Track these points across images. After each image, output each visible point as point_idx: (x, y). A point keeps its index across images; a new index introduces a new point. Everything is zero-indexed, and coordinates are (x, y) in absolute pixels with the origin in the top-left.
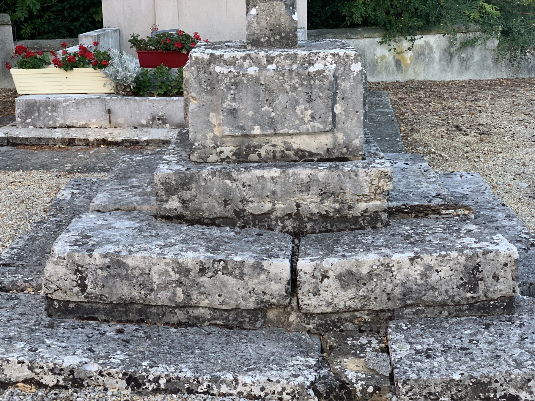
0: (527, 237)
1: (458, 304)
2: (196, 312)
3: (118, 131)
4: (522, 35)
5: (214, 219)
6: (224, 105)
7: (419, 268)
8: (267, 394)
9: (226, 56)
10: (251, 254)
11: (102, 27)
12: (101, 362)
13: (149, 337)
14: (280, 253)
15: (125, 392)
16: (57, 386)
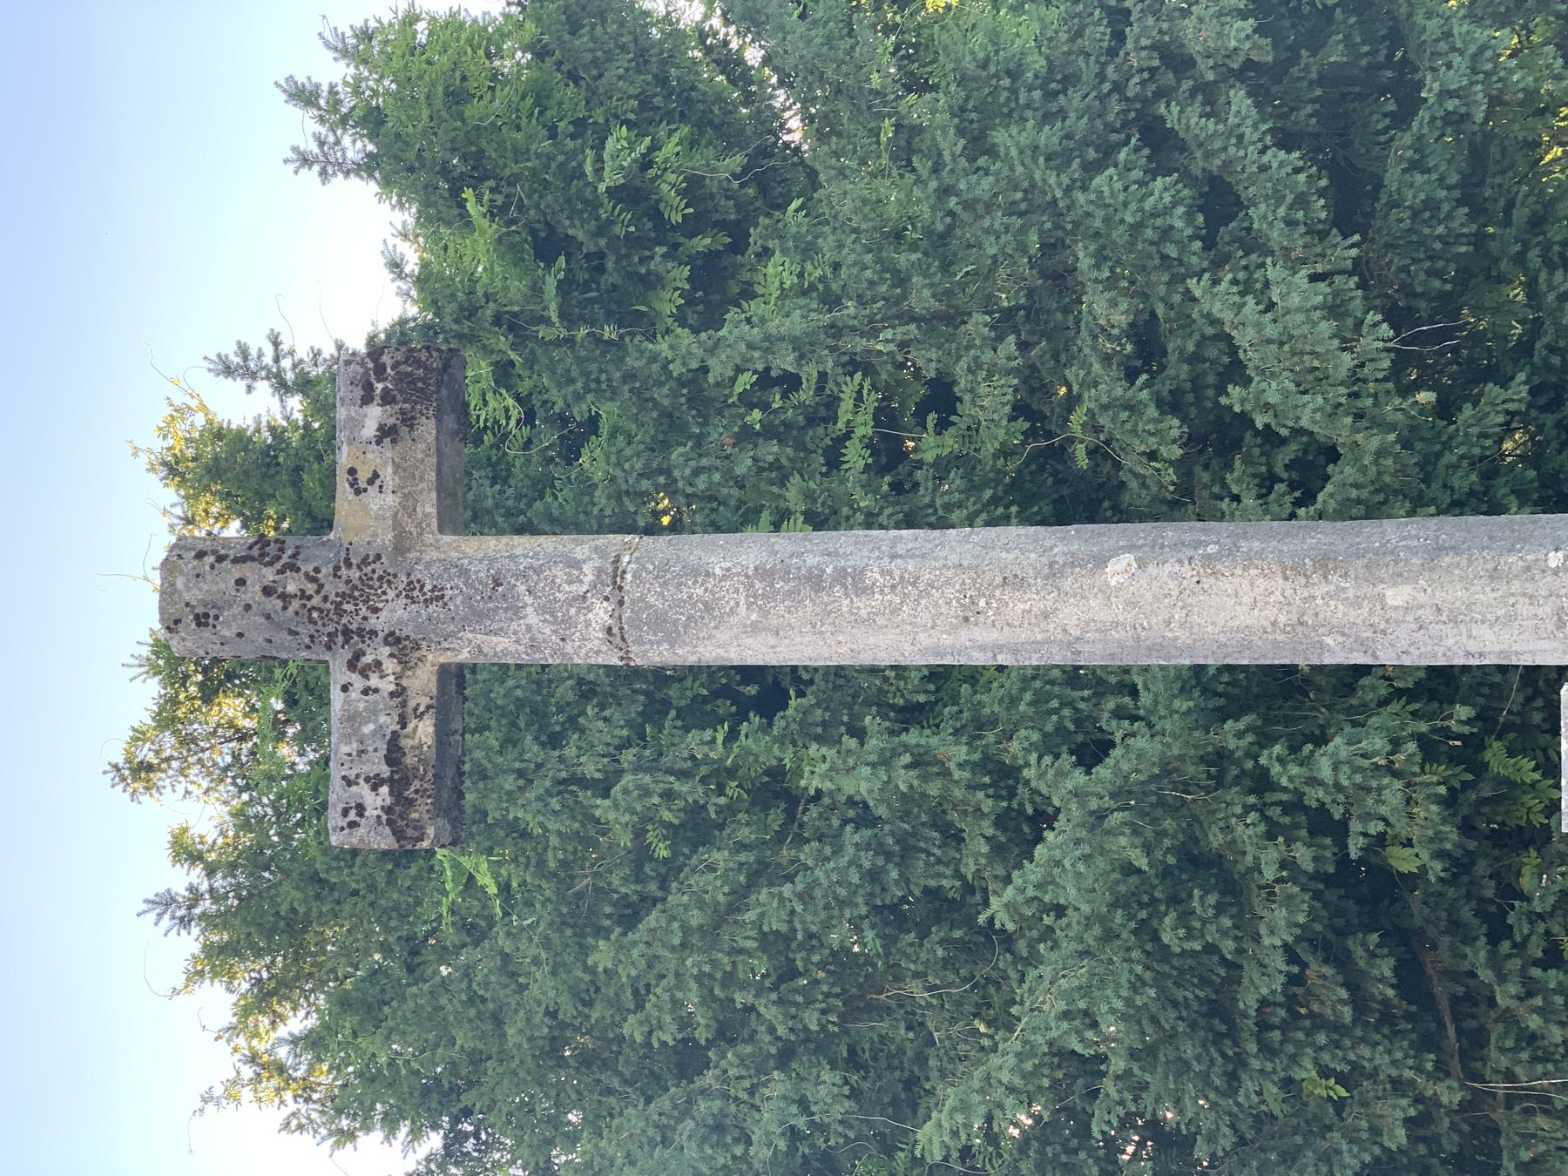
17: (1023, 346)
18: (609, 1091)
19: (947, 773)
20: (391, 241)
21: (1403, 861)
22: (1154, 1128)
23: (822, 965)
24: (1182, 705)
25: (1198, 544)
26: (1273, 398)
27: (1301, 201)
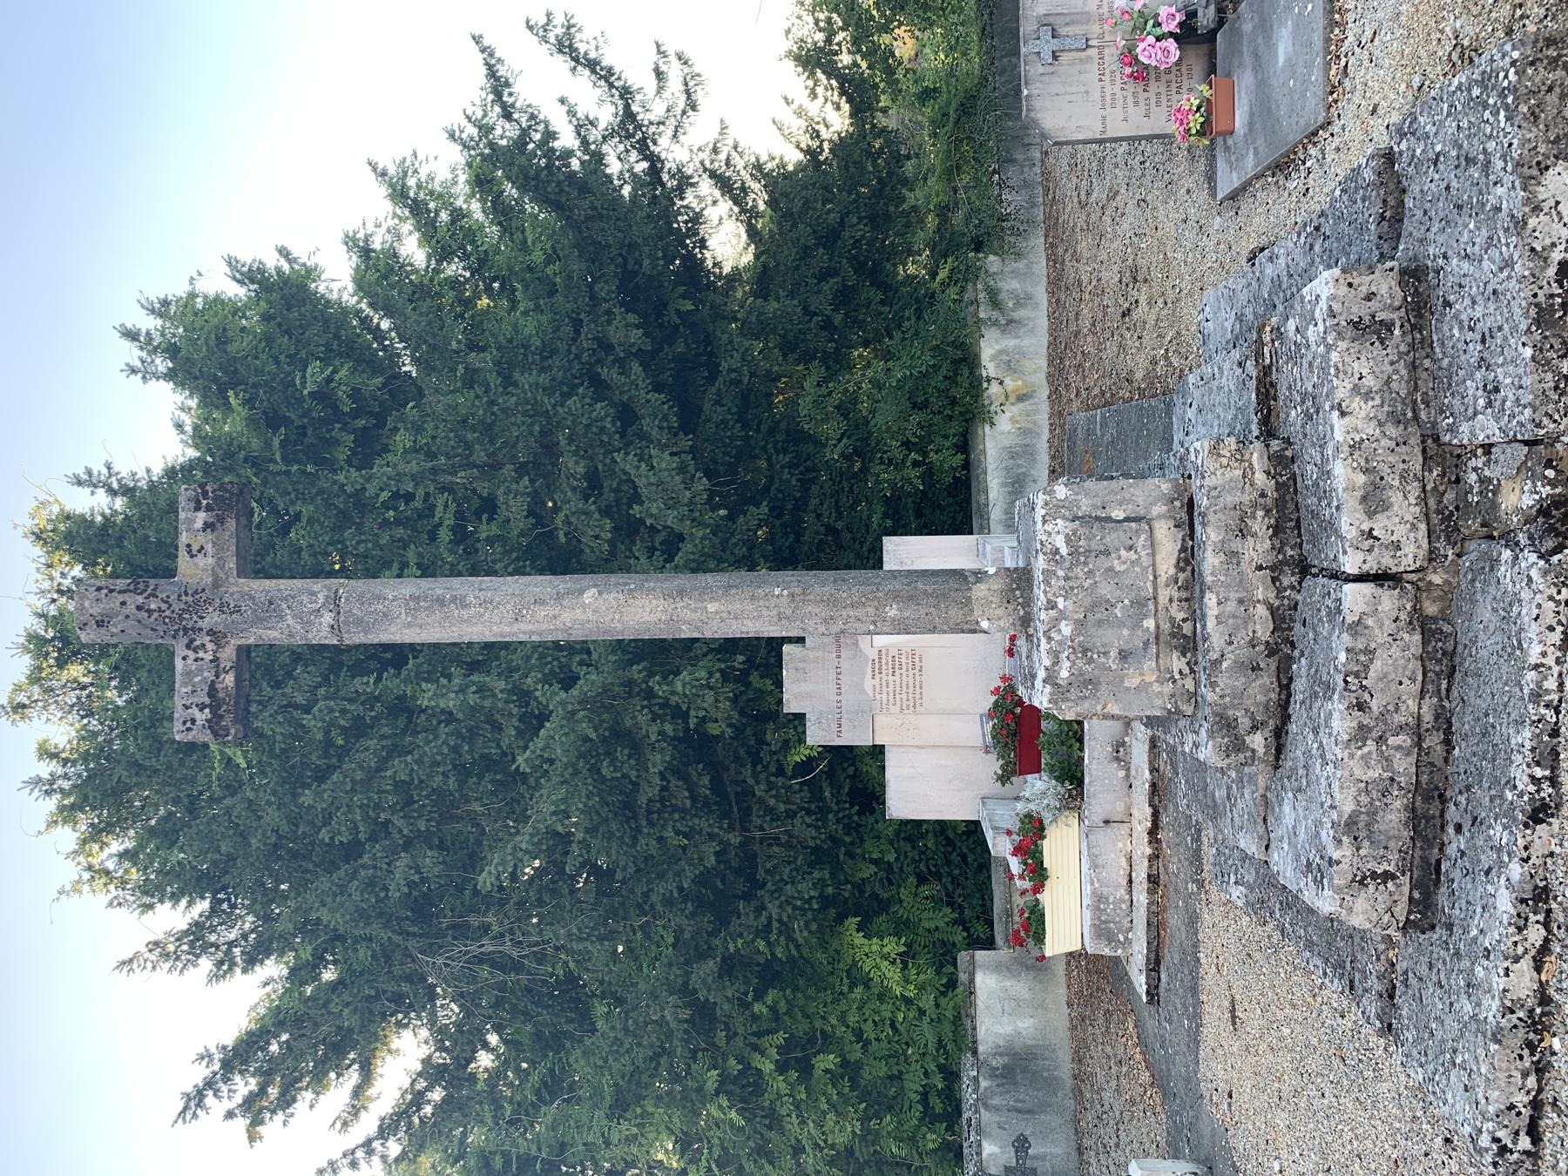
0: (1303, 235)
1: (1412, 346)
2: (1428, 718)
3: (1135, 812)
4: (981, 222)
5: (1280, 686)
6: (1114, 667)
7: (1356, 404)
8: (1560, 623)
9: (1047, 662)
10: (1334, 638)
11: (977, 823)
12: (1506, 859)
13: (1468, 788)
14: (1333, 596)
15: (1556, 826)
16: (1546, 925)
17: (532, 481)
18: (307, 871)
19: (494, 696)
20: (178, 412)
21: (714, 729)
22: (595, 870)
23: (427, 797)
24: (612, 658)
25: (626, 584)
26: (655, 511)
27: (665, 418)
